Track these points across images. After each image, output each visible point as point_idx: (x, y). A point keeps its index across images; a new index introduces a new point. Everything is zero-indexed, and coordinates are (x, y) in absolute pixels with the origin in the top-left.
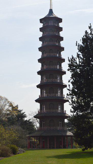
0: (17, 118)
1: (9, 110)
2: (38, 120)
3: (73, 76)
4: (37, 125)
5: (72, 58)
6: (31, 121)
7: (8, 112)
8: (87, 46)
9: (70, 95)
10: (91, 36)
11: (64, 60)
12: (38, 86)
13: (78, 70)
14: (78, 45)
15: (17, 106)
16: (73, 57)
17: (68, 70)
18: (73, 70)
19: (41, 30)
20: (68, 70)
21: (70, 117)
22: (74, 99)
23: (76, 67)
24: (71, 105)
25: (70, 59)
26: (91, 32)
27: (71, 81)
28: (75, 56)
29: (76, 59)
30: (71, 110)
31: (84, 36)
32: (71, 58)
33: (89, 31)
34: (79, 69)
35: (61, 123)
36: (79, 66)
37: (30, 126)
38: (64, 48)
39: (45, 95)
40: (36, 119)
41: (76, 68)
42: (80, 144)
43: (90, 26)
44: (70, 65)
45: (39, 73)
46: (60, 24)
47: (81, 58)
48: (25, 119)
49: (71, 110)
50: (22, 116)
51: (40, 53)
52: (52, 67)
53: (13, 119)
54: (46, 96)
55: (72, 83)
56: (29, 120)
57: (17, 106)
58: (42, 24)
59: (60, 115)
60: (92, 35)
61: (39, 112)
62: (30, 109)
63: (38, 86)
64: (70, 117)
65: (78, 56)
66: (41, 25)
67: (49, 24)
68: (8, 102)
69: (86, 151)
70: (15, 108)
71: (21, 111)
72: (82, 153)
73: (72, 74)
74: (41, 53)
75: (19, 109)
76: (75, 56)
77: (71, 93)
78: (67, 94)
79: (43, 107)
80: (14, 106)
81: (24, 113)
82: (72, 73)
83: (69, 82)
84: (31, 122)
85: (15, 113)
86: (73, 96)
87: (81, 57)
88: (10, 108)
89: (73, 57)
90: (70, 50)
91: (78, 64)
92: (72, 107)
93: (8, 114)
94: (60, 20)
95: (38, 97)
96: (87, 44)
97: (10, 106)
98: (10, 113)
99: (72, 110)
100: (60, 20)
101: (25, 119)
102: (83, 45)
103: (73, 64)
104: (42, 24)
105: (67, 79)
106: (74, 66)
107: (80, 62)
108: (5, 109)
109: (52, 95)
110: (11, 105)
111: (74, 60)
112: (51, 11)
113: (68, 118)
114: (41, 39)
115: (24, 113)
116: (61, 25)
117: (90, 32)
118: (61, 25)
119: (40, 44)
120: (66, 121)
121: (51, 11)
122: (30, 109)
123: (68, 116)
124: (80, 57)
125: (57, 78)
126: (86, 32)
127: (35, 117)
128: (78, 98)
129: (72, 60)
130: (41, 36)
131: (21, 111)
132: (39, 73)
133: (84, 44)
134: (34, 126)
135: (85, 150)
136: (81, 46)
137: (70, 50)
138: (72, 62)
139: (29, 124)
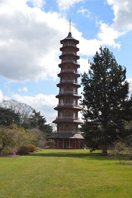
0: (38, 121)
1: (33, 116)
2: (56, 125)
3: (85, 89)
4: (55, 129)
5: (85, 74)
6: (50, 125)
7: (32, 117)
8: (97, 64)
9: (82, 104)
10: (101, 56)
11: (79, 76)
12: (57, 97)
13: (89, 84)
14: (90, 63)
15: (39, 113)
16: (85, 73)
17: (81, 84)
18: (85, 84)
19: (61, 49)
20: (81, 84)
21: (83, 123)
22: (85, 108)
23: (87, 81)
24: (82, 113)
25: (83, 75)
26: (102, 52)
27: (83, 93)
28: (87, 72)
29: (87, 75)
30: (82, 117)
31: (95, 56)
32: (84, 73)
33: (99, 52)
34: (90, 83)
35: (75, 128)
36: (90, 80)
37: (49, 129)
38: (78, 41)
39: (62, 104)
40: (55, 124)
41: (87, 82)
42: (89, 147)
43: (100, 48)
44: (83, 80)
45: (58, 85)
46: (77, 45)
47: (92, 74)
48: (46, 124)
49: (82, 117)
50: (43, 121)
51: (60, 69)
52: (69, 81)
53: (35, 123)
54: (63, 105)
55: (84, 95)
56: (49, 124)
57: (39, 113)
58: (62, 45)
59: (67, 107)
60: (103, 55)
61: (57, 118)
62: (51, 118)
63: (57, 97)
64: (83, 123)
65: (90, 72)
66: (61, 46)
67: (68, 45)
68: (32, 109)
69: (93, 152)
70: (37, 115)
71: (42, 117)
72: (90, 154)
73: (84, 88)
74: (58, 99)
75: (40, 115)
76: (87, 72)
77: (82, 103)
78: (80, 104)
79: (61, 114)
80: (37, 112)
81: (44, 119)
82: (84, 86)
83: (82, 94)
84: (50, 126)
85: (37, 119)
86: (85, 105)
87: (92, 73)
88: (34, 114)
89: (85, 73)
90: (84, 67)
91: (89, 79)
92: (83, 115)
93: (31, 119)
94: (77, 42)
95: (57, 106)
96: (97, 62)
97: (33, 112)
98: (33, 118)
99: (83, 117)
100: (77, 42)
101: (46, 124)
102: (94, 63)
103: (85, 79)
104: (62, 45)
105: (81, 91)
106: (86, 81)
107: (91, 77)
108: (29, 115)
109: (68, 104)
110: (34, 111)
111: (86, 75)
112: (70, 34)
113: (82, 124)
114: (60, 57)
115: (44, 119)
116: (78, 46)
117: (101, 52)
118: (78, 46)
119: (59, 70)
120: (80, 126)
121: (70, 34)
122: (51, 118)
123: (81, 122)
124: (91, 73)
125: (73, 103)
126: (97, 53)
127: (53, 122)
128: (88, 108)
129: (84, 75)
130: (60, 63)
131: (42, 117)
132: (58, 85)
133: (95, 63)
134: (52, 130)
135: (92, 151)
136: (93, 65)
137: (84, 67)
138: (84, 77)
139: (49, 128)
